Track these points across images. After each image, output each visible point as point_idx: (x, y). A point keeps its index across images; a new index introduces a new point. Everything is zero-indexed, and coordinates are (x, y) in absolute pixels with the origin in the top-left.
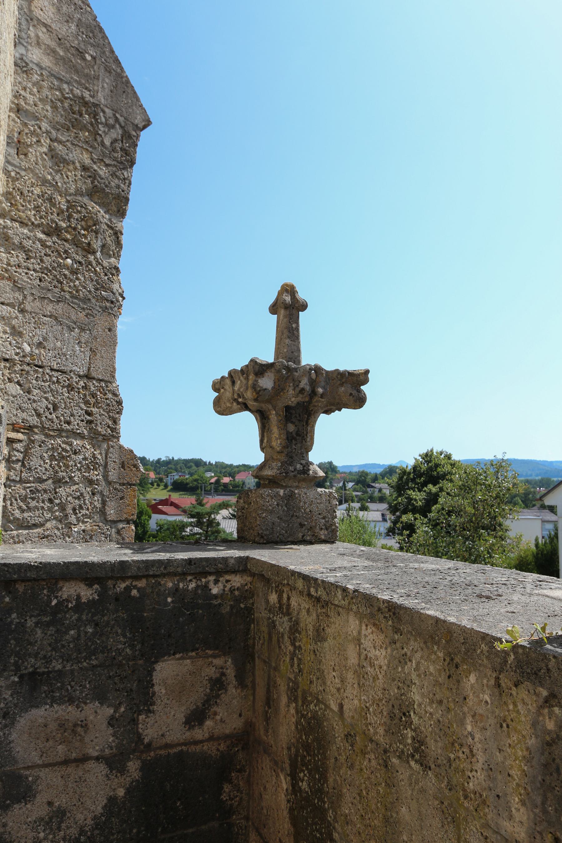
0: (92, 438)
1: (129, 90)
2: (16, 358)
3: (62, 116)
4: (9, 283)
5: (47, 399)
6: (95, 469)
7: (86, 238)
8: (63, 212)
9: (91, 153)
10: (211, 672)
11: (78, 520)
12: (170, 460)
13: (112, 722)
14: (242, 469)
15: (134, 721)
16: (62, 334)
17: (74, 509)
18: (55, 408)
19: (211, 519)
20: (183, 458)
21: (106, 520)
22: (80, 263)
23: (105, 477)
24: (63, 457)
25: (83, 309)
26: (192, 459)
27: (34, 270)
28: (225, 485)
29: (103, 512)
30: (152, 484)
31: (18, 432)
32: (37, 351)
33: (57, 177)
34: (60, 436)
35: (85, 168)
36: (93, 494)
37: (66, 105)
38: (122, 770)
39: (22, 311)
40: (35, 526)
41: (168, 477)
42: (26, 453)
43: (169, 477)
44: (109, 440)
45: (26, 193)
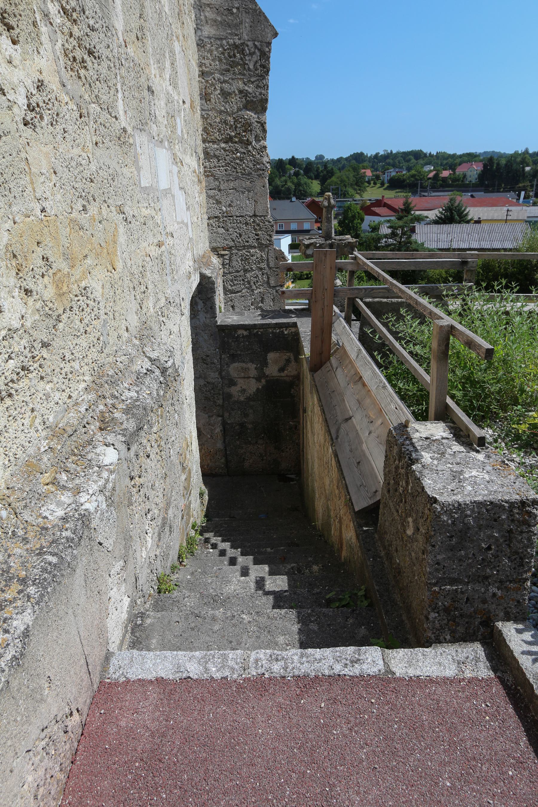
0: (260, 247)
1: (262, 18)
2: (220, 215)
3: (224, 64)
4: (211, 178)
5: (236, 232)
6: (263, 262)
7: (245, 136)
8: (232, 126)
9: (243, 79)
10: (286, 357)
11: (257, 288)
12: (388, 154)
13: (256, 368)
14: (466, 159)
15: (263, 369)
16: (240, 197)
17: (254, 283)
18: (241, 235)
19: (404, 231)
20: (402, 150)
21: (270, 286)
22: (244, 153)
23: (268, 265)
24: (247, 259)
25: (249, 179)
26: (412, 151)
27: (223, 166)
28: (444, 179)
29: (268, 283)
30: (369, 182)
31: (225, 250)
32: (229, 209)
33: (227, 106)
34: (244, 249)
35: (241, 92)
36: (263, 274)
37: (226, 55)
38: (260, 381)
39: (220, 190)
40: (238, 292)
41: (384, 174)
42: (230, 260)
43: (386, 174)
44: (268, 246)
45: (213, 124)
